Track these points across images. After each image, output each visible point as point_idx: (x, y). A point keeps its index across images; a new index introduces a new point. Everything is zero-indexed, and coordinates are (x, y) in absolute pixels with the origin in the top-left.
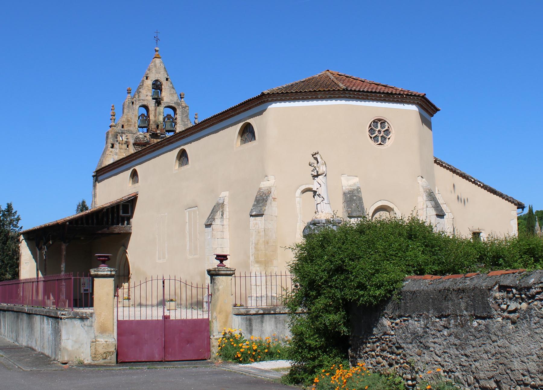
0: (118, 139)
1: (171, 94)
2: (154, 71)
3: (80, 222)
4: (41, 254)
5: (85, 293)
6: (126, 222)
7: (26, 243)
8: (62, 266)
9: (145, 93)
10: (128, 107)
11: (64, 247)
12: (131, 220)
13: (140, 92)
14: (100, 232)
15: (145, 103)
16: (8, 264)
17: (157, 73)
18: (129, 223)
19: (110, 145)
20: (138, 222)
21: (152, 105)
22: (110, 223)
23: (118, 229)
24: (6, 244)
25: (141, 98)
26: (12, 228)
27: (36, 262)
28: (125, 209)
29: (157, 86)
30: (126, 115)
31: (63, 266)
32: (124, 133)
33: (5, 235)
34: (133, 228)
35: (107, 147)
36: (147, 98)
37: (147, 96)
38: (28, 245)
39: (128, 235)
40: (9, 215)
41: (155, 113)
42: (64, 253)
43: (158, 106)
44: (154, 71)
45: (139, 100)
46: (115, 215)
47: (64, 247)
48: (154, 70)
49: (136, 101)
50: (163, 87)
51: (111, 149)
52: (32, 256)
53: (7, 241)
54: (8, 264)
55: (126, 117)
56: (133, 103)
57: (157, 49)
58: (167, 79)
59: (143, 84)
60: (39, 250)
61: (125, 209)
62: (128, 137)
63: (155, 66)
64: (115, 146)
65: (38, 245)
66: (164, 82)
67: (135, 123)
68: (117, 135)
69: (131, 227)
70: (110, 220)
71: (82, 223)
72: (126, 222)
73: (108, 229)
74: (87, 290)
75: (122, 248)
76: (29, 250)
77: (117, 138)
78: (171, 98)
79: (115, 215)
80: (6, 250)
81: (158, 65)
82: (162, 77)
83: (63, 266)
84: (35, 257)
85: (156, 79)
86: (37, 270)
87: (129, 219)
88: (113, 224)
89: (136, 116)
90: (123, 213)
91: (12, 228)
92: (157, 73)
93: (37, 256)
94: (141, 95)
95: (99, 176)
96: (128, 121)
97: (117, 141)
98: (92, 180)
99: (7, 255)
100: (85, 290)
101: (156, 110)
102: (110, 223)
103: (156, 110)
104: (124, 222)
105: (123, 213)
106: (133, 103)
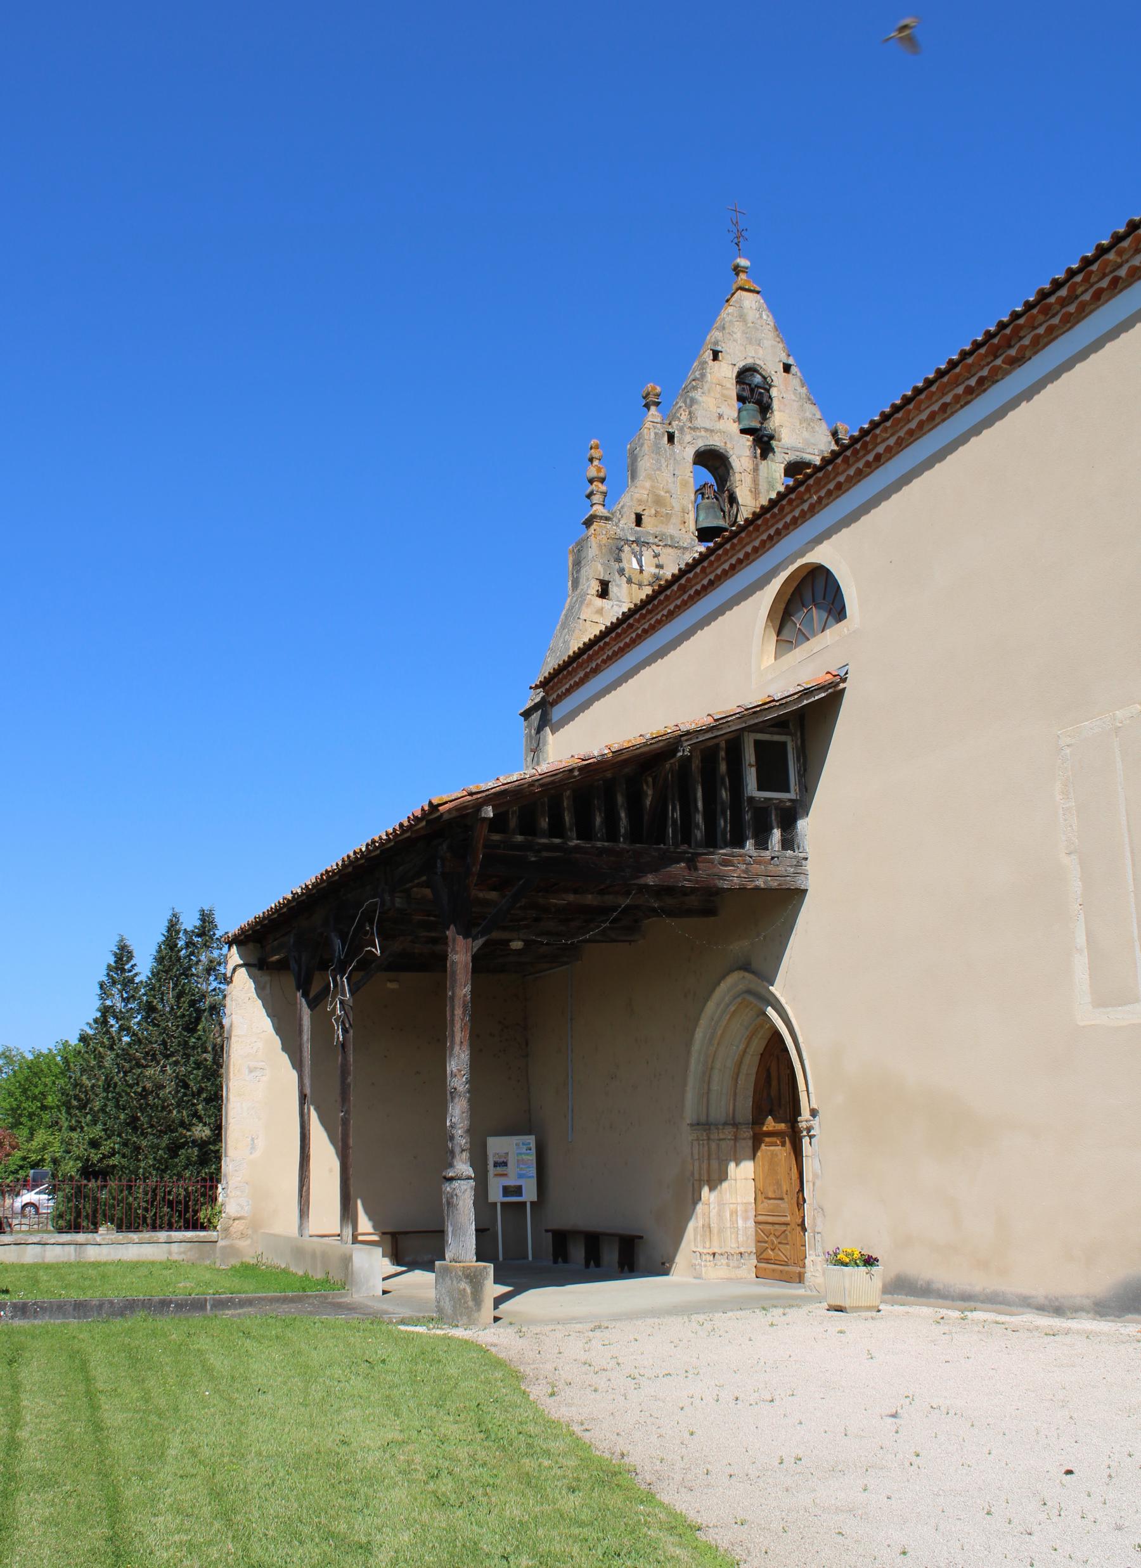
0: (625, 564)
1: (806, 422)
2: (738, 336)
3: (544, 823)
4: (322, 1028)
5: (503, 1204)
6: (777, 834)
7: (251, 985)
8: (452, 1066)
9: (713, 409)
10: (657, 449)
11: (461, 955)
12: (802, 824)
13: (693, 401)
14: (650, 880)
15: (716, 442)
16: (201, 1091)
17: (750, 341)
18: (788, 843)
19: (595, 587)
20: (847, 836)
21: (740, 452)
22: (699, 834)
23: (742, 866)
24: (193, 1031)
25: (699, 422)
26: (214, 984)
27: (297, 1064)
28: (795, 734)
29: (753, 391)
30: (650, 477)
31: (458, 1064)
32: (647, 544)
33: (192, 1003)
34: (809, 866)
35: (584, 595)
36: (720, 425)
37: (720, 416)
38: (260, 990)
39: (790, 898)
40: (206, 945)
41: (755, 481)
42: (464, 991)
43: (764, 456)
44: (738, 336)
45: (694, 429)
46: (724, 794)
47: (461, 955)
48: (737, 329)
49: (681, 430)
50: (774, 392)
51: (599, 602)
52: (277, 1041)
53: (198, 1020)
54: (201, 1091)
55: (648, 484)
56: (671, 438)
57: (743, 262)
58: (787, 368)
59: (703, 376)
60: (312, 1005)
61: (769, 759)
62: (662, 560)
63: (742, 317)
64: (613, 589)
65: (304, 985)
66: (778, 378)
67: (684, 511)
68: (620, 550)
69: (800, 862)
70: (699, 819)
71: (557, 828)
72: (777, 834)
73: (692, 864)
74: (518, 1191)
75: (733, 982)
76: (259, 913)
77: (619, 560)
78: (806, 434)
79: (724, 794)
80: (194, 1048)
81: (752, 315)
82: (769, 355)
83: (458, 1064)
84: (291, 1046)
85: (750, 361)
86: (303, 1098)
87: (789, 817)
88: (712, 841)
89: (684, 484)
90: (760, 788)
91: (214, 984)
92: (750, 341)
93: (301, 1032)
94: (699, 413)
95: (554, 704)
96: (658, 501)
97: (621, 572)
98: (522, 728)
99: (198, 1065)
100: (507, 1191)
101: (756, 469)
102: (699, 834)
103: (756, 469)
104: (768, 831)
105: (760, 788)
106: (671, 438)
